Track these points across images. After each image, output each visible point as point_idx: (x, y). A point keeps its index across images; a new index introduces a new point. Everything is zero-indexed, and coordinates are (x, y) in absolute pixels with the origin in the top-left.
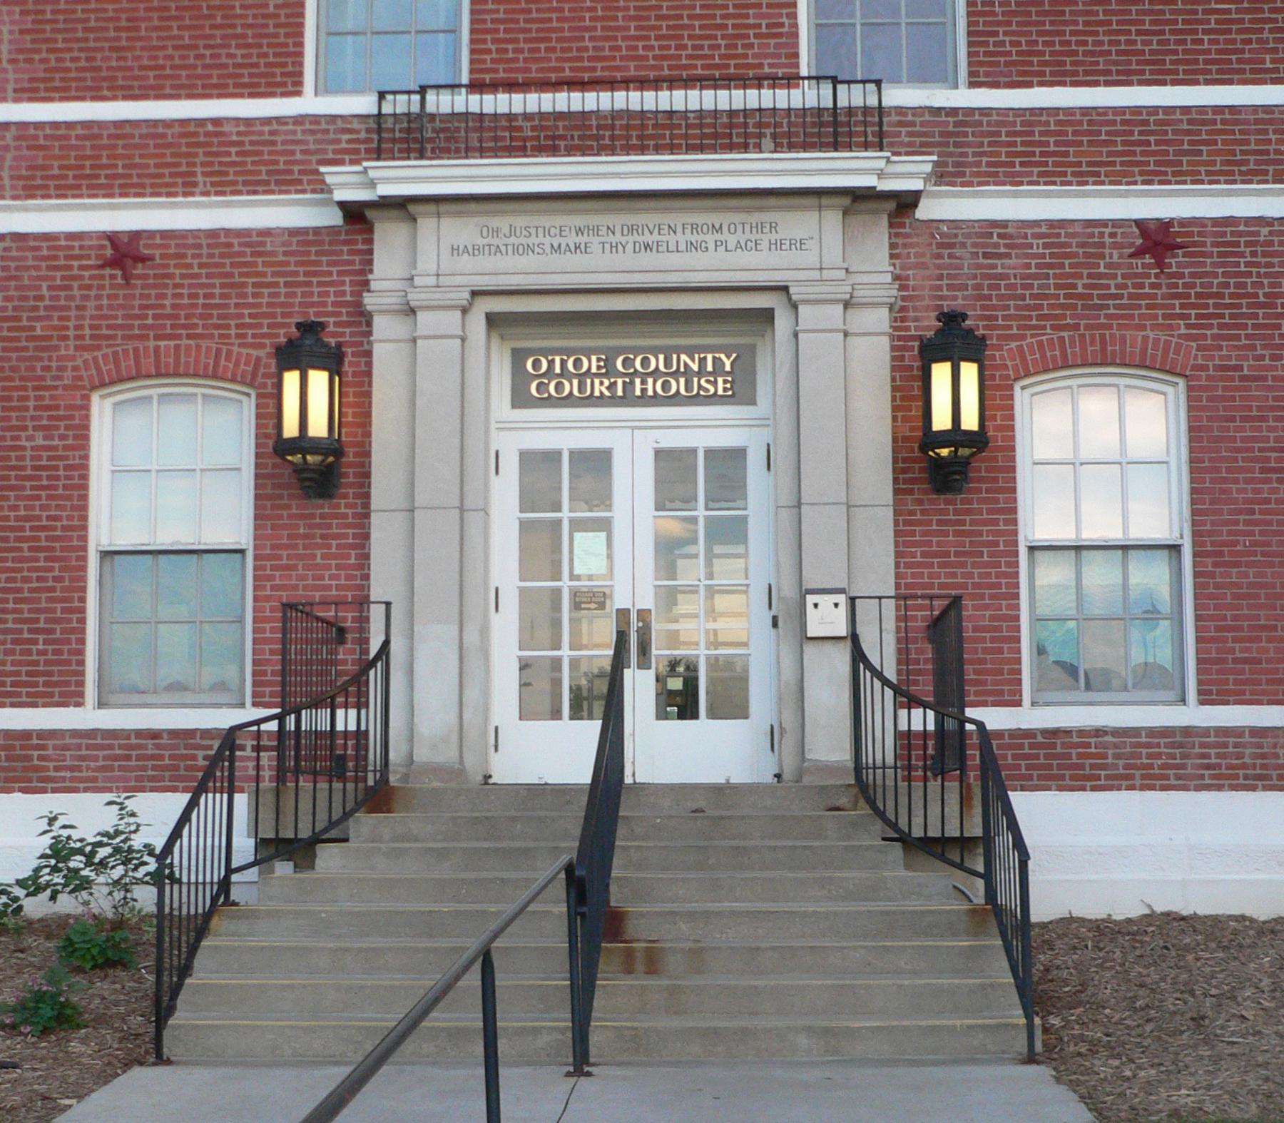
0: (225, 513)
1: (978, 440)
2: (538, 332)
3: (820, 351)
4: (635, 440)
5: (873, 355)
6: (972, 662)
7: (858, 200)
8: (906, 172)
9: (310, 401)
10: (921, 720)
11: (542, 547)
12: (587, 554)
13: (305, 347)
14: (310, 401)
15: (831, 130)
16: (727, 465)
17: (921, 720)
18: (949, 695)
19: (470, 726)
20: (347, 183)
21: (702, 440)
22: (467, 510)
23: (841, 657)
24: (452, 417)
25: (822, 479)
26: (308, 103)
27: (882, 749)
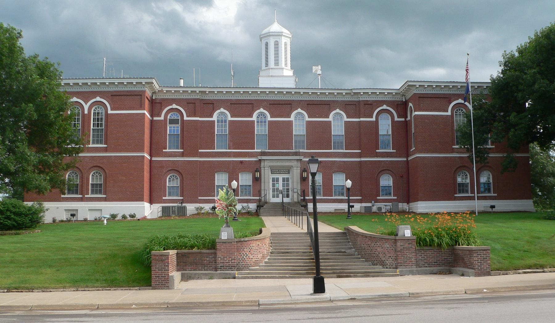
0: (250, 182)
1: (306, 178)
2: (274, 170)
3: (295, 171)
4: (281, 177)
5: (299, 171)
6: (313, 259)
7: (297, 160)
8: (301, 158)
9: (258, 175)
10: (302, 198)
11: (274, 185)
12: (277, 186)
13: (256, 171)
14: (258, 175)
15: (296, 154)
16: (288, 179)
17: (302, 198)
18: (304, 197)
19: (269, 199)
20: (260, 158)
21: (286, 177)
22: (269, 182)
23: (296, 194)
24: (268, 176)
25: (295, 180)
26: (255, 150)
27: (300, 200)
